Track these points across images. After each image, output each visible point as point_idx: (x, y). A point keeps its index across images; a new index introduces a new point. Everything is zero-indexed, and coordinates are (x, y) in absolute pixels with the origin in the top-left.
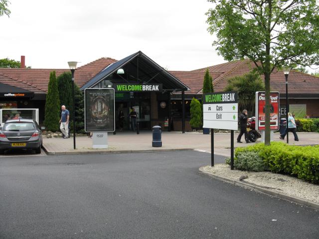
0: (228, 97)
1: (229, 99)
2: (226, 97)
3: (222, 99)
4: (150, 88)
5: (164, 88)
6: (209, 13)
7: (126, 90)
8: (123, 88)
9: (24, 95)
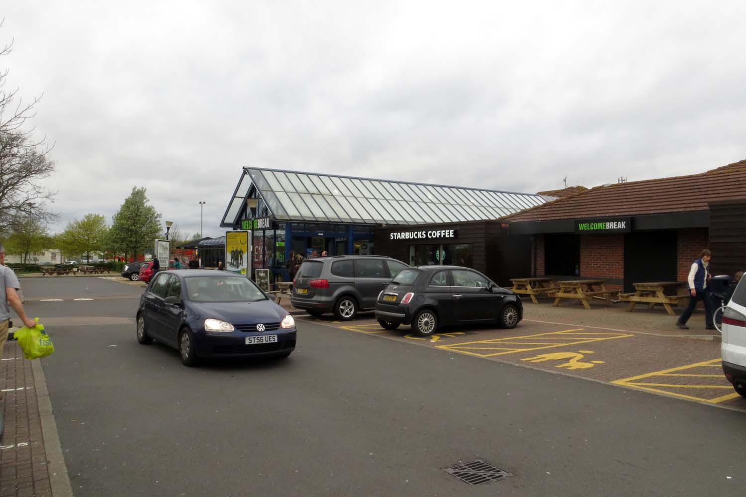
0: (263, 223)
1: (264, 225)
2: (261, 223)
3: (257, 226)
4: (615, 225)
6: (196, 316)
7: (588, 229)
8: (585, 226)
9: (622, 225)
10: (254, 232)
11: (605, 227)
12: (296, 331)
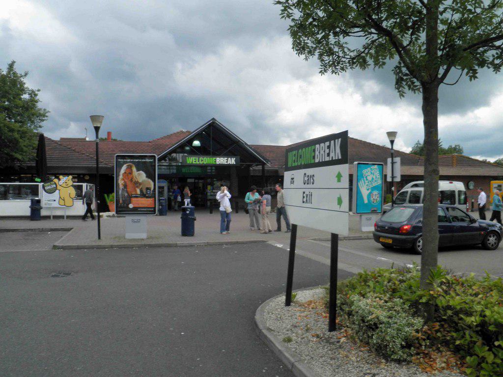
0: (327, 151)
1: (328, 155)
2: (322, 152)
3: (314, 157)
5: (242, 160)
7: (197, 163)
10: (394, 158)
11: (215, 162)
12: (100, 127)
